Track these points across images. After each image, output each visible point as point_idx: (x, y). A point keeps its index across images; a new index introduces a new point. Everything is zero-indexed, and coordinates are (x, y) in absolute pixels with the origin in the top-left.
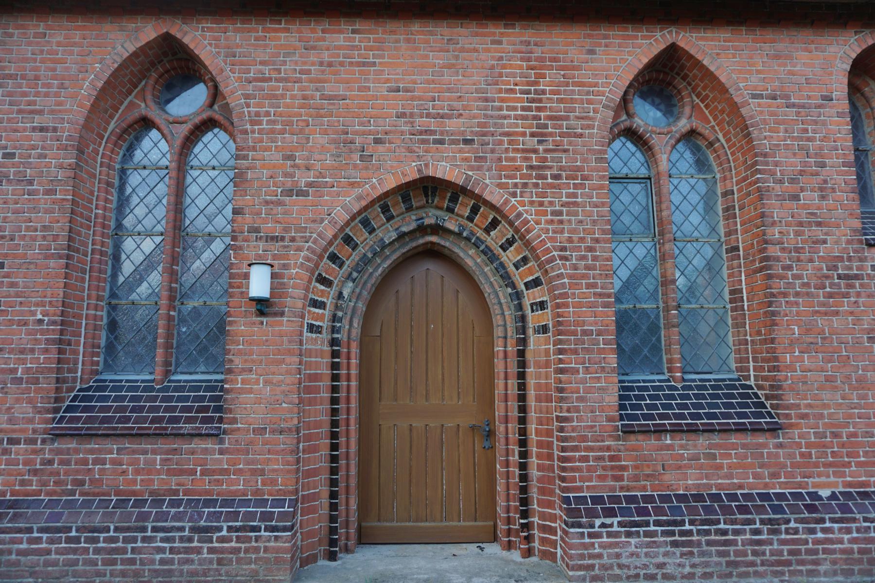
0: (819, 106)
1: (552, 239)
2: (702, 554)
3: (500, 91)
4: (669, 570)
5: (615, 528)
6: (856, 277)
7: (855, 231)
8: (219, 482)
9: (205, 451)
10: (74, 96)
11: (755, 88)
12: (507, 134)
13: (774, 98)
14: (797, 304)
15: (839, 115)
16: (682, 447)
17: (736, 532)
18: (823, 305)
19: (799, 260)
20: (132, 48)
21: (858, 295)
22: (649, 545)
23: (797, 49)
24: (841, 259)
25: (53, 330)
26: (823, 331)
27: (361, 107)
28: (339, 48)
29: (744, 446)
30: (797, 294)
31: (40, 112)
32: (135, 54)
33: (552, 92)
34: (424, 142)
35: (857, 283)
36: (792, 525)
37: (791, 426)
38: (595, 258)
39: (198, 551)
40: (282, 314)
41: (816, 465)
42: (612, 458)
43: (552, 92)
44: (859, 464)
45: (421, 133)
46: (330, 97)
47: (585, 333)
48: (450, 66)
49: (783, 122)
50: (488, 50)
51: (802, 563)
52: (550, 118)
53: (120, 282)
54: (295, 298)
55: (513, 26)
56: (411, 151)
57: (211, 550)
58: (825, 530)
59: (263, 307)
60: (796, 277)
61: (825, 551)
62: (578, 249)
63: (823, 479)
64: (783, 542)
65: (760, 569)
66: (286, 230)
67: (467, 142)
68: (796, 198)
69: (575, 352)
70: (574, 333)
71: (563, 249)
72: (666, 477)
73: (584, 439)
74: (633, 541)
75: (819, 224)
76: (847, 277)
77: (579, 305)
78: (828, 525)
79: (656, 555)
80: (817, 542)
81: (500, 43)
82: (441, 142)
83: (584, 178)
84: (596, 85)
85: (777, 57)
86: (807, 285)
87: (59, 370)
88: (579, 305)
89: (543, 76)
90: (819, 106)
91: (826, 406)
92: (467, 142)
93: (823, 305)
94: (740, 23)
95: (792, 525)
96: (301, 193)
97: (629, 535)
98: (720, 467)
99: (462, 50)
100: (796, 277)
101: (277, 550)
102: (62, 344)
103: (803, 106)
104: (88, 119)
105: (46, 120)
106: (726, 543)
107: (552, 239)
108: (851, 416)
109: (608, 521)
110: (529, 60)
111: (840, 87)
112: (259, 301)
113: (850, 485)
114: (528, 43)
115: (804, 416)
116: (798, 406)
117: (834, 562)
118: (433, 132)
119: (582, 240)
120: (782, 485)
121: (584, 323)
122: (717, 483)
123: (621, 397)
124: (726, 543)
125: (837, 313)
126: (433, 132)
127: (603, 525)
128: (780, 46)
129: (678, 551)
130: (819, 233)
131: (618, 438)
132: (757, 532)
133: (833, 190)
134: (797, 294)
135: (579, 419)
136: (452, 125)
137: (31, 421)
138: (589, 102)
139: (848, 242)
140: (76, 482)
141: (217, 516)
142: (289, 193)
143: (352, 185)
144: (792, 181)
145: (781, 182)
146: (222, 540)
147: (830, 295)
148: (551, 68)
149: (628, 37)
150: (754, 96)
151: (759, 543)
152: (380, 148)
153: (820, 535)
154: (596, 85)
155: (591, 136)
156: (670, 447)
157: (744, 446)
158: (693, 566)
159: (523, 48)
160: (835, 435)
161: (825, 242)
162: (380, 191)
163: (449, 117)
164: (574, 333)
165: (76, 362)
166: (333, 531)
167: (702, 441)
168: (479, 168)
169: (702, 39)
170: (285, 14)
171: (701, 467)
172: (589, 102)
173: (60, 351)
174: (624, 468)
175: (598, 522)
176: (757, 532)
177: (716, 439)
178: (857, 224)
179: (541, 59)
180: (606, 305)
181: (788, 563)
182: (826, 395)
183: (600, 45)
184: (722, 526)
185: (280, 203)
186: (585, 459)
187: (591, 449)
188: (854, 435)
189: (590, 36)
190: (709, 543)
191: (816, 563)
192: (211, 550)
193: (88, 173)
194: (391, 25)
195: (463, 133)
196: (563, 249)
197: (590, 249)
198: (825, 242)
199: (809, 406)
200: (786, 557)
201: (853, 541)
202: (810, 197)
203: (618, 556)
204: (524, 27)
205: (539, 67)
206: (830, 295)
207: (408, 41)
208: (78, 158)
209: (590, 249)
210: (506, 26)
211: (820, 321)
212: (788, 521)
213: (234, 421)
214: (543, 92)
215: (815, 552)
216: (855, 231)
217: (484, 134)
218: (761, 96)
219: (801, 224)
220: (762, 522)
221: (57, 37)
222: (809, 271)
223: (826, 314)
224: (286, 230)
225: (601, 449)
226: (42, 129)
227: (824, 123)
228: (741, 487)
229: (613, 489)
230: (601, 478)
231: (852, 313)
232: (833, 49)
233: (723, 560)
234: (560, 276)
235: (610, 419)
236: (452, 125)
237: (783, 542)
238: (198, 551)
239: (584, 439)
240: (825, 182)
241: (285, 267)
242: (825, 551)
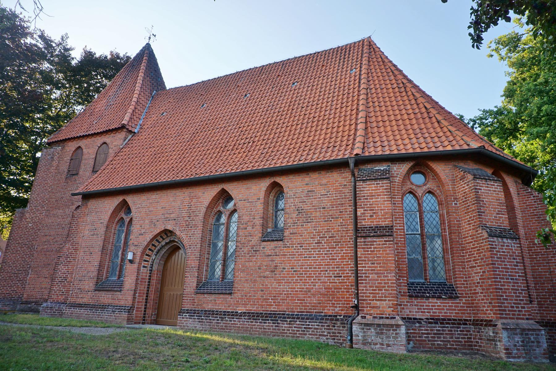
0: (256, 201)
1: (188, 243)
2: (205, 325)
3: (183, 206)
4: (197, 328)
5: (187, 317)
6: (258, 251)
7: (259, 237)
8: (119, 302)
9: (118, 295)
10: (107, 215)
11: (240, 198)
12: (183, 217)
13: (245, 200)
14: (241, 259)
15: (261, 203)
16: (209, 298)
17: (213, 320)
18: (248, 259)
19: (244, 246)
20: (118, 203)
21: (258, 256)
22: (194, 321)
23: (253, 186)
24: (255, 246)
25: (394, 293)
26: (247, 266)
27: (156, 213)
28: (153, 199)
29: (223, 298)
30: (242, 256)
31: (101, 219)
32: (118, 204)
33: (194, 205)
34: (166, 220)
35: (258, 252)
36: (227, 319)
37: (235, 293)
38: (196, 248)
39: (112, 316)
40: (135, 263)
41: (240, 304)
42: (193, 300)
43: (194, 205)
44: (251, 304)
45: (166, 218)
46: (150, 211)
47: (192, 267)
48: (174, 201)
49: (246, 207)
50: (182, 196)
51: (227, 329)
52: (192, 212)
53: (229, 255)
54: (137, 260)
55: (188, 189)
56: (163, 223)
57: (114, 316)
58: (234, 321)
59: (131, 261)
60: (243, 251)
61: (233, 327)
62: (193, 245)
63: (241, 308)
64: (224, 323)
65: (218, 330)
66: (138, 243)
67: (175, 220)
68: (246, 229)
69: (189, 272)
70: (189, 267)
71: (190, 246)
72: (204, 305)
73: (188, 294)
74: (191, 320)
75: (251, 236)
76: (256, 251)
77: (191, 260)
78: (235, 319)
79: (195, 324)
80: (232, 324)
81: (184, 193)
82: (169, 220)
83: (197, 227)
84: (203, 202)
85: (247, 188)
86: (245, 253)
87: (98, 276)
88: (191, 260)
89: (192, 201)
90: (256, 201)
91: (244, 288)
92: (175, 220)
93: (248, 259)
94: (240, 180)
95: (227, 319)
96: (142, 235)
97: (190, 318)
98: (216, 303)
99: (177, 196)
100: (243, 251)
101: (125, 317)
102: (99, 271)
103: (252, 202)
104: (109, 220)
105: (101, 221)
106: (211, 322)
107: (188, 243)
108: (250, 291)
109: (186, 315)
110: (190, 197)
111: (262, 195)
112: (130, 260)
113: (247, 310)
114: (190, 193)
115: (239, 290)
116: (237, 287)
117: (235, 330)
118: (168, 218)
119: (194, 243)
120: (231, 309)
121: (191, 265)
122: (216, 308)
123: (197, 284)
124: (211, 322)
125: (251, 261)
126: (168, 218)
127: (185, 316)
128: (248, 185)
129: (200, 323)
130: (250, 238)
131: (195, 295)
132: (218, 320)
133: (256, 226)
134: (242, 256)
135: (187, 289)
136: (172, 216)
137: (92, 287)
138: (201, 207)
139: (258, 241)
140: (97, 301)
141: (116, 309)
142: (140, 235)
143: (151, 232)
144: (246, 224)
145: (243, 224)
146: (116, 314)
147: (250, 256)
148: (194, 198)
149: (213, 188)
150: (240, 200)
151: (218, 323)
152: (158, 222)
153: (233, 322)
154: (203, 202)
155: (200, 216)
156: (205, 298)
157: (223, 298)
158: (203, 328)
159: (189, 194)
160: (246, 296)
161: (251, 241)
162: (157, 233)
163: (172, 214)
164: (189, 267)
165: (103, 275)
166: (144, 317)
167: (213, 296)
168: (176, 226)
169: (230, 186)
170: (144, 192)
171: (212, 303)
172: (201, 207)
173: (98, 272)
174: (195, 302)
175: (184, 315)
176: (218, 320)
177: (217, 296)
178: (260, 235)
179: (192, 197)
180: (197, 260)
181: (224, 329)
182: (245, 284)
183: (206, 191)
184: (210, 318)
185: (138, 237)
186: (187, 300)
187: (189, 297)
188: (251, 296)
189: (204, 189)
190: (207, 322)
191: (230, 329)
192: (114, 316)
193: (109, 232)
194: (164, 192)
195: (174, 218)
196: (190, 246)
197: (196, 245)
198: (251, 241)
199: (241, 287)
200: (224, 327)
201: (241, 324)
202: (250, 228)
203: (187, 323)
204: (190, 189)
205: (191, 198)
206: (250, 256)
207: (167, 195)
208: (106, 229)
209: (196, 245)
210: (187, 189)
211: (247, 264)
212: (226, 318)
213: (124, 288)
214: (192, 205)
215: (231, 327)
216: (259, 237)
217: (178, 217)
218: (242, 200)
219: (246, 236)
220: (220, 318)
221: (106, 202)
222: (246, 250)
223: (248, 261)
224: (138, 243)
225: (191, 297)
226: (101, 223)
227: (256, 206)
228: (220, 309)
229: (192, 308)
230: (190, 305)
231: (255, 261)
232: (262, 184)
233: (209, 327)
234: (189, 253)
235: (194, 290)
236: (172, 216)
237: (224, 323)
238: (112, 316)
239: (188, 294)
240: (254, 223)
241: (137, 252)
242: (233, 327)
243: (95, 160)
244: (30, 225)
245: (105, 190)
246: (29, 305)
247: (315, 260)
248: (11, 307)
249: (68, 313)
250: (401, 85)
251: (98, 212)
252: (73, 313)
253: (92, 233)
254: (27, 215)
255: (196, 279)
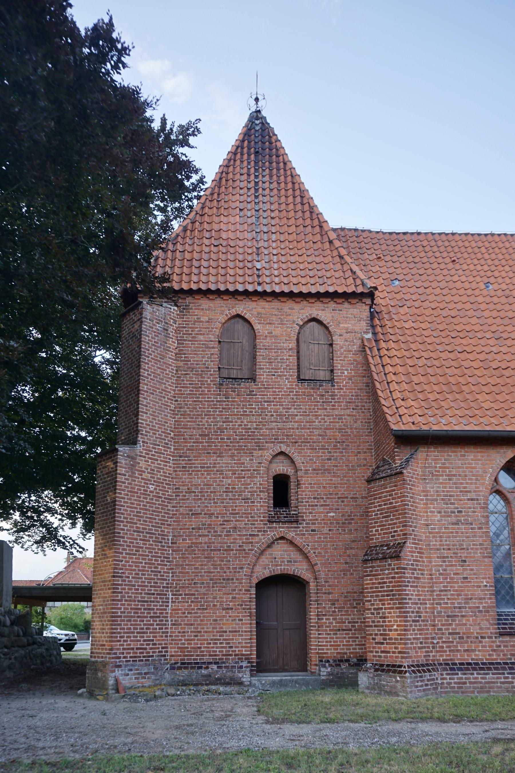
31: (470, 492)
221: (471, 456)
243: (298, 352)
244: (152, 488)
245: (450, 433)
246: (204, 672)
247: (163, 520)
248: (153, 677)
249: (449, 684)
250: (349, 273)
251: (454, 475)
252: (465, 683)
253: (454, 519)
254: (142, 464)
255: (93, 562)
